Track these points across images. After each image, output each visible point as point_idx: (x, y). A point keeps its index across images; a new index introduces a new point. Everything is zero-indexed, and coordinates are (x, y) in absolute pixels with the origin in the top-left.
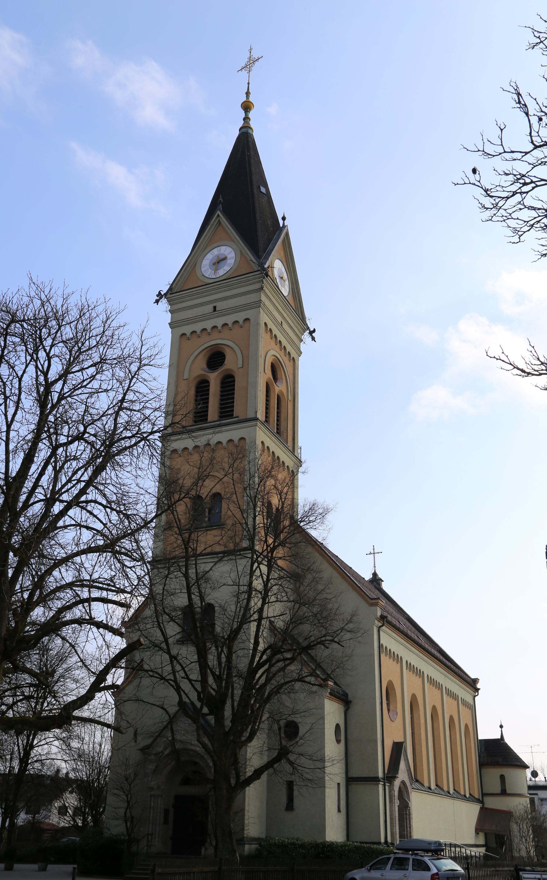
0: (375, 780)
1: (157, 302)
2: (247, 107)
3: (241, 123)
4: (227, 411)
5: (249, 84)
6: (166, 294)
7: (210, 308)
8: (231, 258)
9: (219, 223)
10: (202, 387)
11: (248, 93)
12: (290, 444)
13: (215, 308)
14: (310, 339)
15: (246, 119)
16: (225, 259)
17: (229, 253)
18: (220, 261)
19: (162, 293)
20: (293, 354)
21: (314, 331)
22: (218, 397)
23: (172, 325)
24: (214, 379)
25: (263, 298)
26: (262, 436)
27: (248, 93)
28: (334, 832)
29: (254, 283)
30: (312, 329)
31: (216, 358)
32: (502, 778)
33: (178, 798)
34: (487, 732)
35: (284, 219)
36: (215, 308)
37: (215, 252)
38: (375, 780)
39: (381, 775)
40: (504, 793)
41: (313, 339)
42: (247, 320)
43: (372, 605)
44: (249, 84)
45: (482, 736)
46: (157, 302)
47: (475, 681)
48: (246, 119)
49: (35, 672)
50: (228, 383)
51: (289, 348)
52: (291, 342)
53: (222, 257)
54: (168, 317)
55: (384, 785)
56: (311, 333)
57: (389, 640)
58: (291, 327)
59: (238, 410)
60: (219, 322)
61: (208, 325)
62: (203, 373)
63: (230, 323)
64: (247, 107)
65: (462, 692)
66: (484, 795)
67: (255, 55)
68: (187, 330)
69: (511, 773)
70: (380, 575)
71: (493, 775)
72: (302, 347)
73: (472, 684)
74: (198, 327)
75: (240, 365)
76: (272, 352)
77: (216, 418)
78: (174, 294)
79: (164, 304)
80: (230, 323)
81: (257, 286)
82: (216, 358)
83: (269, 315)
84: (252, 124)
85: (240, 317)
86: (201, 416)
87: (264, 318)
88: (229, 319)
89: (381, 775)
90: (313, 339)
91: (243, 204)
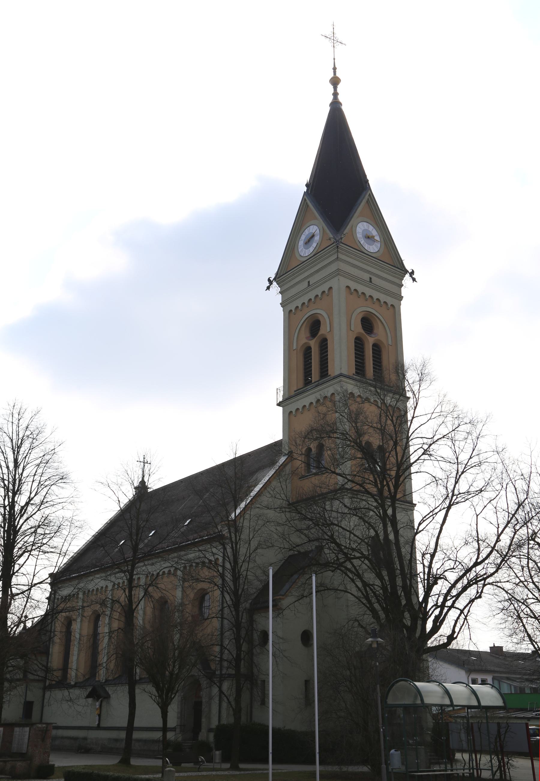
1: (268, 288)
2: (335, 82)
3: (331, 98)
5: (334, 59)
6: (275, 279)
7: (305, 284)
10: (307, 351)
11: (335, 69)
14: (411, 280)
15: (335, 94)
16: (313, 236)
19: (272, 279)
23: (283, 305)
24: (314, 344)
27: (335, 69)
29: (331, 255)
30: (410, 271)
41: (414, 280)
42: (331, 288)
44: (334, 59)
46: (268, 288)
48: (335, 94)
49: (412, 559)
50: (324, 345)
53: (312, 235)
54: (279, 298)
55: (65, 668)
56: (412, 273)
62: (307, 341)
64: (335, 82)
67: (329, 33)
74: (305, 299)
81: (335, 257)
82: (315, 326)
84: (340, 98)
90: (414, 280)
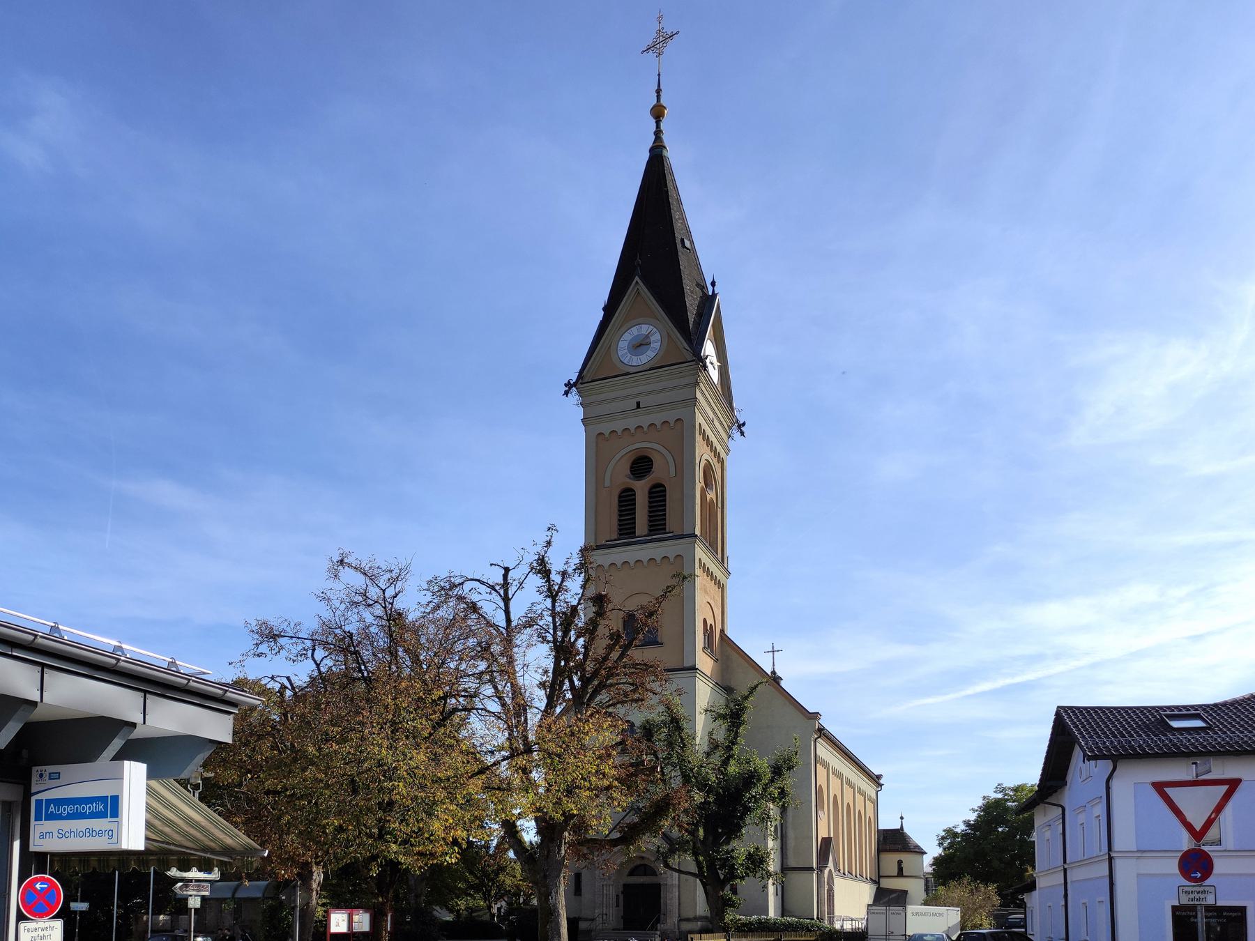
0: (811, 869)
1: (566, 393)
2: (658, 113)
4: (658, 526)
8: (655, 342)
9: (638, 293)
10: (626, 499)
12: (719, 556)
13: (638, 404)
15: (658, 133)
17: (648, 334)
18: (640, 345)
20: (723, 455)
21: (744, 424)
22: (647, 509)
23: (584, 421)
24: (641, 488)
25: (698, 395)
26: (701, 553)
28: (772, 913)
31: (641, 465)
32: (900, 863)
33: (626, 887)
34: (888, 822)
35: (713, 284)
36: (638, 404)
37: (635, 331)
38: (811, 869)
39: (815, 866)
40: (900, 874)
41: (742, 434)
43: (810, 718)
45: (884, 825)
46: (566, 393)
47: (879, 777)
48: (658, 133)
50: (658, 494)
51: (719, 448)
52: (721, 441)
56: (740, 426)
57: (823, 750)
58: (721, 424)
59: (671, 523)
60: (645, 421)
61: (632, 423)
63: (658, 424)
64: (658, 113)
65: (869, 788)
66: (880, 877)
67: (669, 30)
68: (606, 428)
69: (906, 858)
70: (779, 674)
71: (890, 860)
72: (731, 443)
73: (876, 780)
75: (672, 473)
76: (706, 456)
77: (646, 532)
78: (582, 383)
79: (574, 397)
80: (658, 424)
82: (641, 465)
83: (706, 413)
85: (671, 416)
86: (626, 530)
87: (699, 419)
88: (657, 418)
89: (815, 866)
90: (742, 434)
91: (655, 260)
